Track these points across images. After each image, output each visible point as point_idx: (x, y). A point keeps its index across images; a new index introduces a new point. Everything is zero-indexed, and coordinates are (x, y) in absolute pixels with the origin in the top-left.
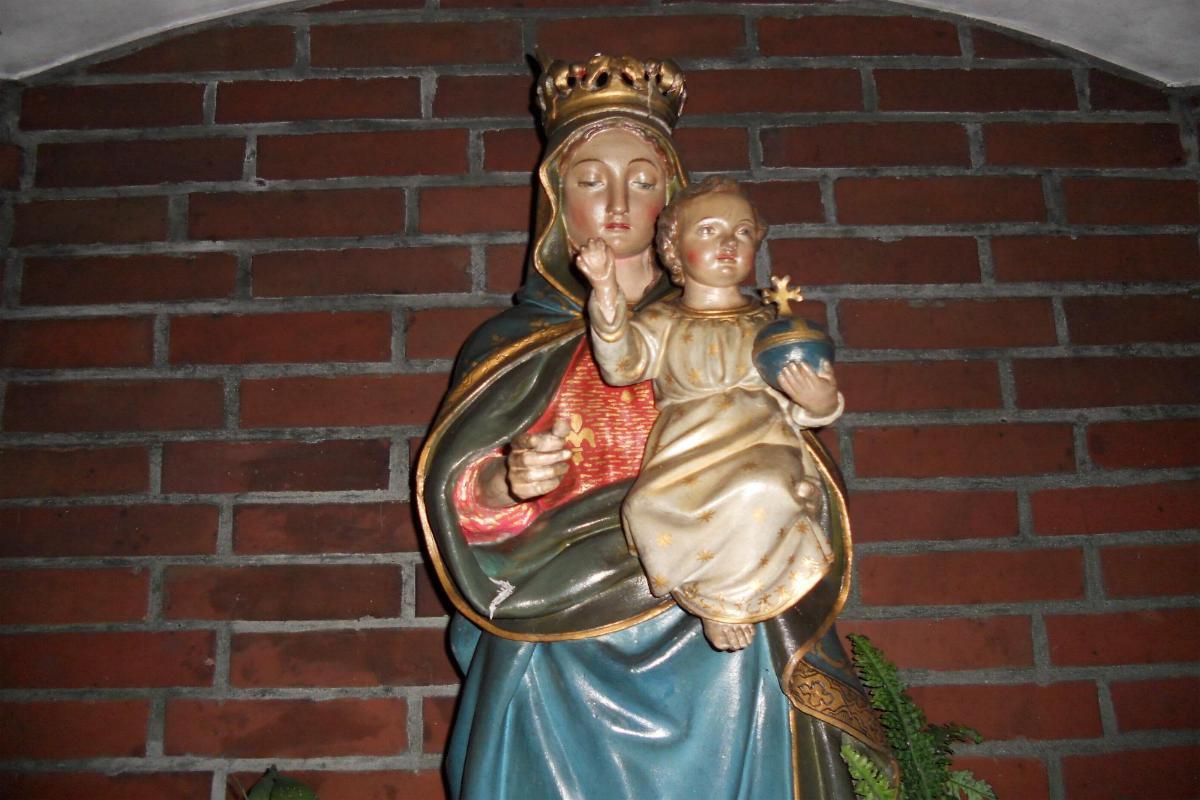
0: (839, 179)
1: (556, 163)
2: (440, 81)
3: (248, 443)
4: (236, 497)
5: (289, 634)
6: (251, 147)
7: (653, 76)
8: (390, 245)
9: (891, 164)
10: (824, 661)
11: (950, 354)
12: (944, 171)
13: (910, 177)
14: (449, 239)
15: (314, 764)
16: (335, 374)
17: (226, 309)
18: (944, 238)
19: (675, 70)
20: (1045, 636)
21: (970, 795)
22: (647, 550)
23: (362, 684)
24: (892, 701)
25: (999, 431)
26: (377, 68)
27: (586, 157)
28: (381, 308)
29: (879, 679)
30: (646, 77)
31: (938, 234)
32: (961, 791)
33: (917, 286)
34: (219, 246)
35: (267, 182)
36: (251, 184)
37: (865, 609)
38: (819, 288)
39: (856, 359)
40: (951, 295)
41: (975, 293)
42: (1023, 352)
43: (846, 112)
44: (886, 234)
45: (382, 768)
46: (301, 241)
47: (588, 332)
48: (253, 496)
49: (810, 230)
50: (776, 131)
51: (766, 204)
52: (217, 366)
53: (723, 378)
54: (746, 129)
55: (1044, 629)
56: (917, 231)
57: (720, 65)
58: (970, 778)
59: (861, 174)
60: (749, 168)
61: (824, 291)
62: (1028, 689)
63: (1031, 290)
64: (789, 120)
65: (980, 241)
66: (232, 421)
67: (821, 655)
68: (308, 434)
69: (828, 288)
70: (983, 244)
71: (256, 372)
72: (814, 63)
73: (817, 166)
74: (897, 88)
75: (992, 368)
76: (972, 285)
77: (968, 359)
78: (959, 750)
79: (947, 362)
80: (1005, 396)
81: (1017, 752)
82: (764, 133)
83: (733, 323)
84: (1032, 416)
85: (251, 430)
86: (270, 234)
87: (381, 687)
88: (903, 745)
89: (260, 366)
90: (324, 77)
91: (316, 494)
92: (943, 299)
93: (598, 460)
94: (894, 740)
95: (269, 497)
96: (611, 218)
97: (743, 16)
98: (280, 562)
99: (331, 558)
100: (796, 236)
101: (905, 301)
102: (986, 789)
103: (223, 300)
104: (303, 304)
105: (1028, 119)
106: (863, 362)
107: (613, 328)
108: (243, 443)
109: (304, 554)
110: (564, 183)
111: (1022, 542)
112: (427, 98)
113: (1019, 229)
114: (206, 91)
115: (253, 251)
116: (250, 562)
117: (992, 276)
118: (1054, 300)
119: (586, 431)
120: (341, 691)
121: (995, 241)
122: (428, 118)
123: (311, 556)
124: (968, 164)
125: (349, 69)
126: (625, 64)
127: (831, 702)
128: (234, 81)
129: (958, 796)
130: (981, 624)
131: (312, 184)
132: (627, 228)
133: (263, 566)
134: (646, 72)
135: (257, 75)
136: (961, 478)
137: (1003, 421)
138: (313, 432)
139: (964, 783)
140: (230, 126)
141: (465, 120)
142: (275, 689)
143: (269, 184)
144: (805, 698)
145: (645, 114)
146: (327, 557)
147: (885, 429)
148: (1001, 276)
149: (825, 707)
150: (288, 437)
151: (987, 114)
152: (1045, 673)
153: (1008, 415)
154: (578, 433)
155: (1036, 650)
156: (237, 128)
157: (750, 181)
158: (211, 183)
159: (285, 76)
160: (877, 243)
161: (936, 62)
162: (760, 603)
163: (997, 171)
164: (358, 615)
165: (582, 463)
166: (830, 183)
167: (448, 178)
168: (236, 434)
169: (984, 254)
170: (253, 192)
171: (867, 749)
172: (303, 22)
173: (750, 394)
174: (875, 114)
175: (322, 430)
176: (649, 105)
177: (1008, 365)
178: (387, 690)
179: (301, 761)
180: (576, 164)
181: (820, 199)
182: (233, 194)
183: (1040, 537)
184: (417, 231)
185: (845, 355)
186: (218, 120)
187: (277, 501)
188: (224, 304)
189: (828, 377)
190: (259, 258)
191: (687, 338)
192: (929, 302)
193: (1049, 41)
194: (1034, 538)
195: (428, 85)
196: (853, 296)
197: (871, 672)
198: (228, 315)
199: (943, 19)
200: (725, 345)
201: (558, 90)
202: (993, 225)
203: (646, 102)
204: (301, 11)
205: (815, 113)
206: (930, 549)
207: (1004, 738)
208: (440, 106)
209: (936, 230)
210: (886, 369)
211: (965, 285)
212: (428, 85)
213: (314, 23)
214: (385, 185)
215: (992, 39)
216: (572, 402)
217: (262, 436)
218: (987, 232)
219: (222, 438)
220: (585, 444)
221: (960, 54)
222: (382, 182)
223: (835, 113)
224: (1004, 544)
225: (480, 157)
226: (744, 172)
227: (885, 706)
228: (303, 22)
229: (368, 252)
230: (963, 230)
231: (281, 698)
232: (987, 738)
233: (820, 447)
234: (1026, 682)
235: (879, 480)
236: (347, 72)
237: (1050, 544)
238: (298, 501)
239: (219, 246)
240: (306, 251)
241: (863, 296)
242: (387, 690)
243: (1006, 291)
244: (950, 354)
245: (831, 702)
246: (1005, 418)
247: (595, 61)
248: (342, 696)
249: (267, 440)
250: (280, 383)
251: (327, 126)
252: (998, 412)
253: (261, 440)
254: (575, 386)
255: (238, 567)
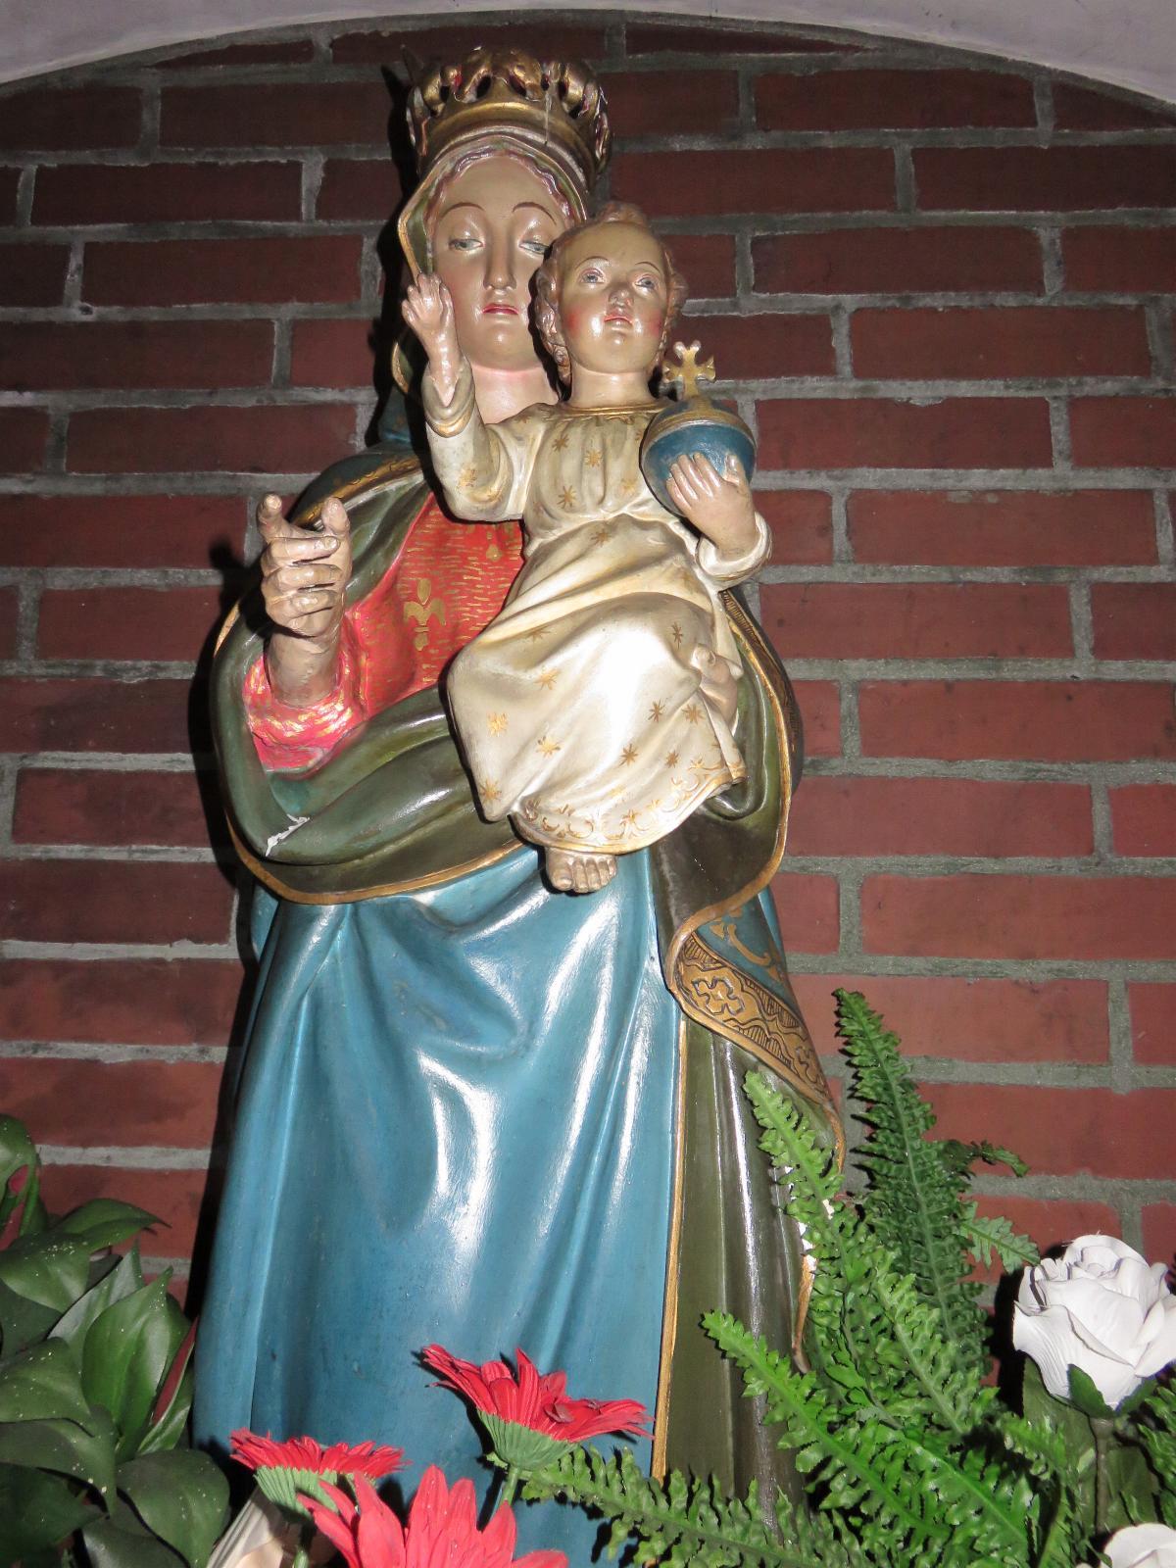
0: (858, 310)
1: (420, 216)
2: (329, 167)
3: (44, 680)
4: (25, 757)
5: (76, 962)
6: (75, 261)
7: (553, 82)
8: (250, 402)
9: (931, 287)
10: (735, 949)
11: (1004, 574)
12: (1008, 300)
13: (957, 309)
14: (329, 395)
15: (96, 1156)
16: (167, 585)
17: (29, 489)
18: (1000, 399)
19: (586, 77)
20: (1128, 1016)
21: (1005, 1256)
22: (474, 741)
23: (168, 1041)
24: (887, 1088)
25: (1068, 691)
26: (247, 149)
27: (457, 202)
28: (234, 492)
29: (871, 1055)
30: (545, 85)
31: (994, 394)
32: (993, 1252)
33: (961, 471)
34: (27, 399)
35: (95, 309)
36: (75, 312)
37: (868, 959)
38: (823, 474)
39: (870, 579)
40: (1009, 485)
41: (1043, 484)
42: (1108, 574)
43: (871, 213)
44: (919, 392)
45: (187, 1167)
46: (136, 394)
47: (495, 523)
48: (46, 758)
49: (814, 387)
50: (774, 239)
51: (693, 264)
52: (13, 568)
53: (601, 501)
54: (734, 237)
55: (1126, 1002)
56: (965, 389)
57: (701, 145)
58: (1006, 1230)
59: (889, 303)
60: (735, 294)
61: (830, 477)
62: (1099, 1097)
63: (1124, 479)
64: (794, 223)
65: (1053, 405)
66: (26, 647)
67: (733, 940)
68: (126, 670)
69: (837, 472)
70: (1057, 409)
71: (64, 579)
72: (829, 140)
73: (828, 294)
74: (944, 177)
75: (1060, 596)
76: (1040, 471)
77: (1027, 582)
78: (984, 1183)
79: (996, 585)
80: (1077, 638)
81: (1076, 1194)
82: (756, 242)
83: (626, 422)
84: (1116, 670)
85: (51, 662)
86: (91, 383)
87: (195, 1046)
88: (899, 1155)
89: (70, 570)
90: (177, 161)
91: (130, 756)
92: (997, 492)
93: (448, 644)
94: (886, 1147)
95: (66, 760)
96: (490, 295)
97: (736, 72)
98: (73, 856)
99: (143, 851)
100: (796, 396)
101: (944, 492)
102: (1029, 1249)
103: (28, 476)
104: (131, 484)
105: (1128, 222)
106: (879, 584)
107: (449, 412)
108: (37, 680)
109: (106, 845)
110: (433, 250)
111: (1097, 864)
112: (309, 190)
113: (1109, 387)
114: (21, 179)
115: (71, 406)
116: (34, 855)
117: (1069, 457)
118: (1156, 494)
119: (435, 603)
120: (141, 1050)
121: (1075, 404)
122: (309, 221)
123: (116, 848)
124: (1040, 290)
125: (208, 149)
126: (513, 60)
127: (738, 1011)
128: (59, 166)
129: (988, 1261)
130: (1034, 990)
131: (153, 314)
132: (514, 313)
133: (51, 861)
134: (544, 76)
135: (88, 157)
136: (1011, 762)
137: (1073, 677)
138: (134, 668)
139: (997, 1237)
140: (50, 228)
141: (359, 223)
142: (52, 1044)
143: (97, 312)
144: (701, 1001)
145: (540, 139)
146: (137, 851)
147: (905, 683)
148: (1081, 459)
149: (729, 1016)
150: (99, 673)
151: (1070, 213)
152: (1125, 1074)
153: (1082, 667)
154: (425, 607)
155: (1113, 1037)
156: (58, 232)
157: (735, 314)
158: (21, 310)
159: (127, 159)
160: (907, 406)
161: (1000, 137)
162: (624, 823)
163: (1081, 300)
164: (169, 938)
165: (426, 648)
166: (845, 317)
167: (333, 306)
168: (30, 667)
169: (1058, 424)
170: (75, 323)
171: (794, 1094)
172: (152, 83)
173: (645, 526)
174: (915, 215)
175: (145, 664)
176: (546, 126)
177: (1084, 592)
178: (202, 1052)
179: (78, 1150)
180: (446, 213)
181: (830, 341)
182: (50, 324)
183: (1124, 858)
184: (288, 382)
185: (854, 573)
186: (34, 222)
187: (76, 766)
188: (30, 482)
189: (737, 481)
190: (78, 418)
191: (560, 444)
192: (979, 494)
193: (1163, 102)
194: (1117, 860)
195: (312, 176)
196: (872, 486)
197: (860, 1043)
198: (33, 498)
199: (1013, 72)
200: (611, 451)
201: (429, 105)
202: (1073, 381)
203: (543, 120)
204: (151, 67)
205: (829, 215)
206: (963, 869)
207: (1060, 1171)
208: (326, 207)
209: (992, 388)
210: (911, 593)
211: (1030, 471)
212: (312, 176)
213: (168, 84)
214: (248, 316)
215: (1085, 102)
216: (420, 561)
217: (66, 672)
218: (1063, 392)
219: (12, 672)
220: (432, 621)
221: (1034, 124)
222: (245, 312)
223: (857, 214)
224: (1070, 866)
225: (375, 278)
226: (727, 300)
227: (877, 1094)
228: (152, 83)
229: (224, 412)
230: (1030, 388)
231: (58, 1056)
232: (1032, 1170)
233: (760, 638)
234: (1097, 1085)
235: (895, 761)
236: (207, 153)
237: (1139, 871)
238: (105, 766)
239: (27, 399)
240: (140, 409)
241: (886, 485)
242: (202, 1052)
243: (1090, 479)
244: (1004, 574)
245: (738, 1011)
246: (1077, 674)
247: (475, 58)
248: (141, 1057)
249: (72, 676)
250: (93, 596)
251: (175, 231)
252: (1067, 663)
253: (62, 676)
254: (426, 538)
255: (17, 860)
